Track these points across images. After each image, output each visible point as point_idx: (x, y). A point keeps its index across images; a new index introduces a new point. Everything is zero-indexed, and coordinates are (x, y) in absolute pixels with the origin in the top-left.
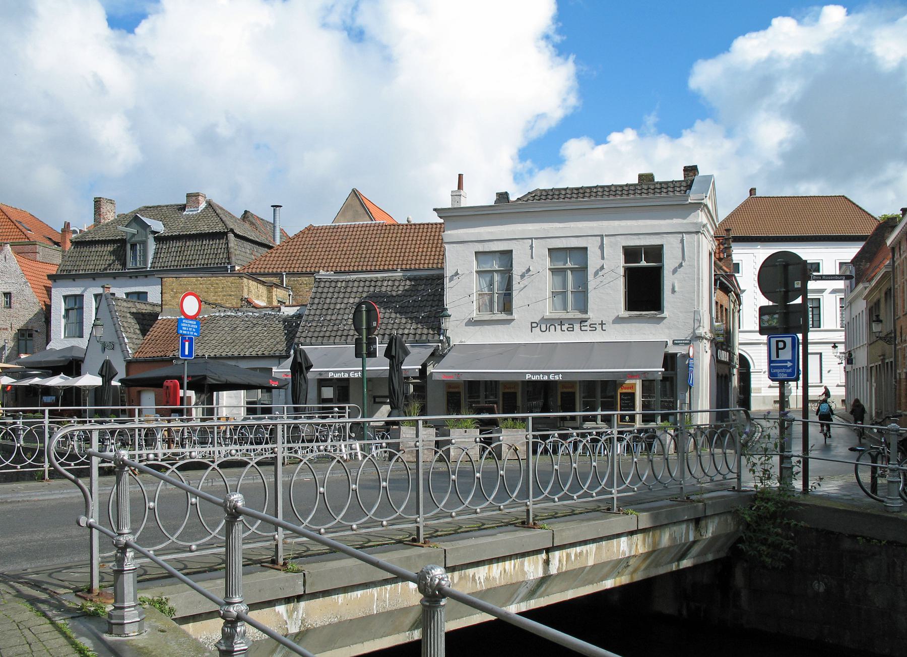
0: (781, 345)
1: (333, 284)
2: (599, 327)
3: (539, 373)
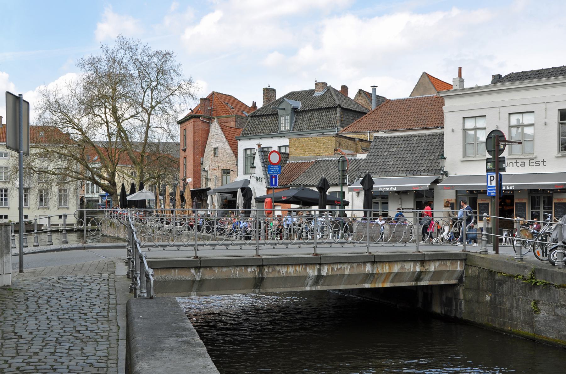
2: (542, 164)
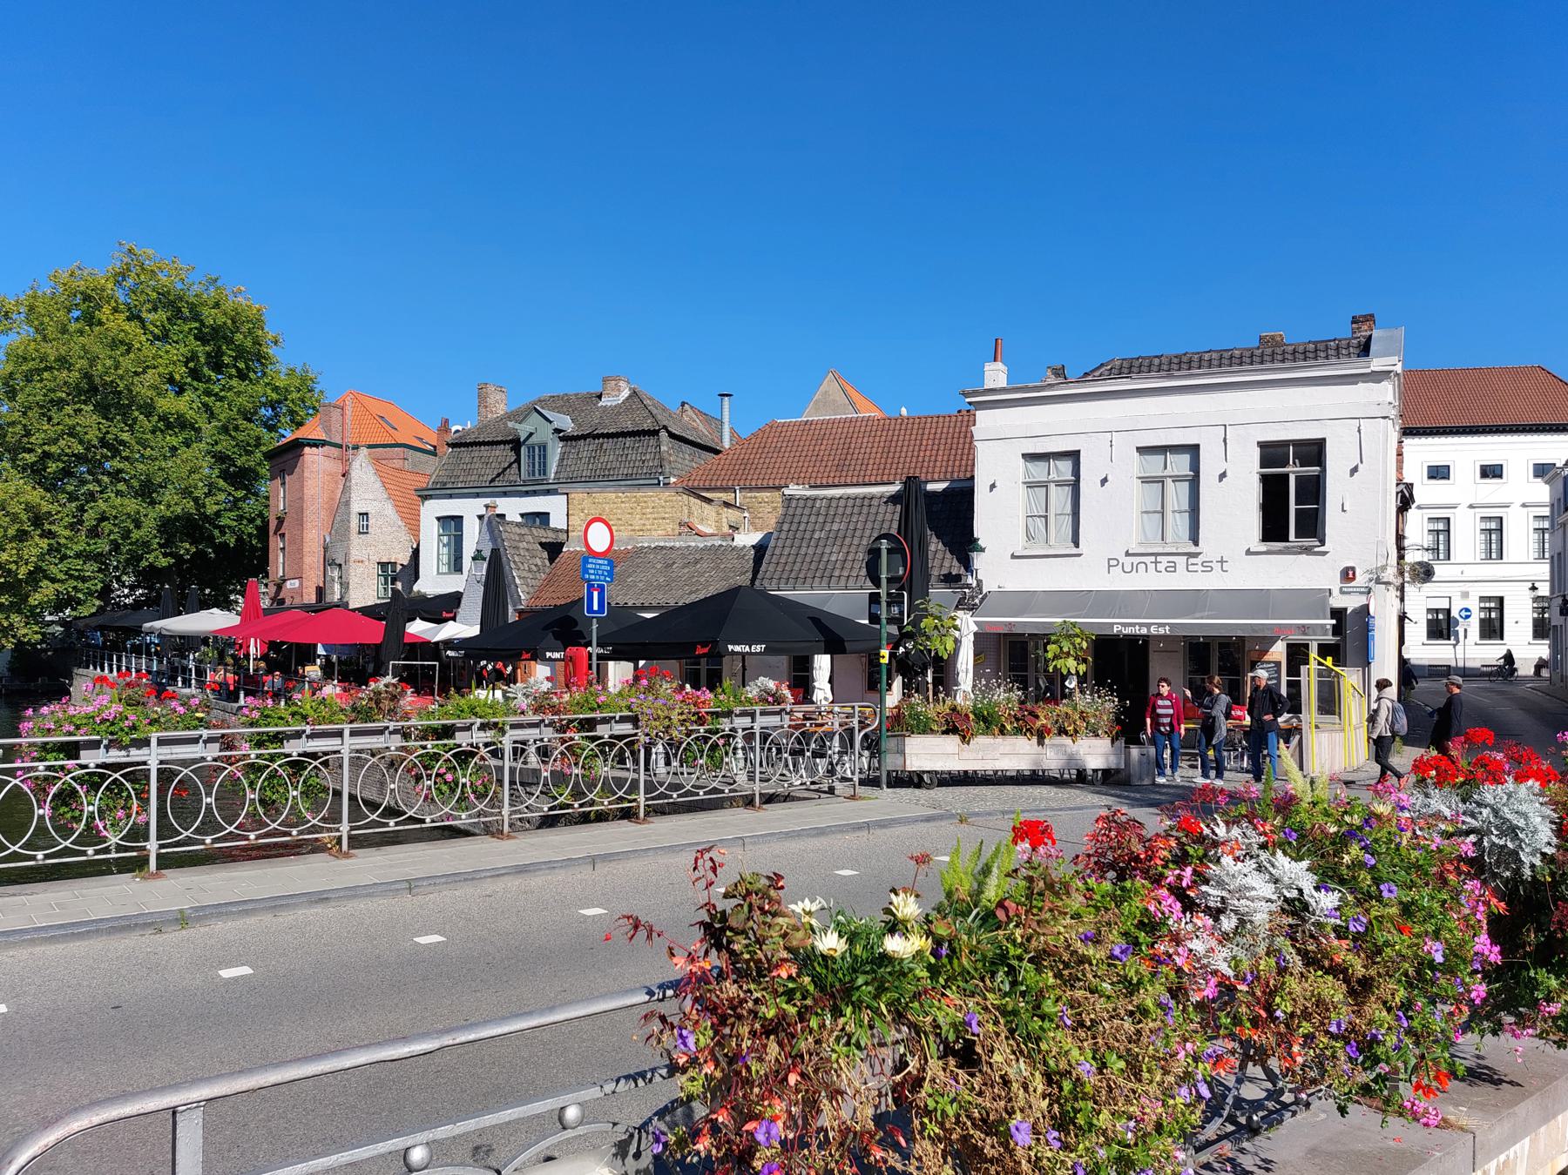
3: (1133, 625)
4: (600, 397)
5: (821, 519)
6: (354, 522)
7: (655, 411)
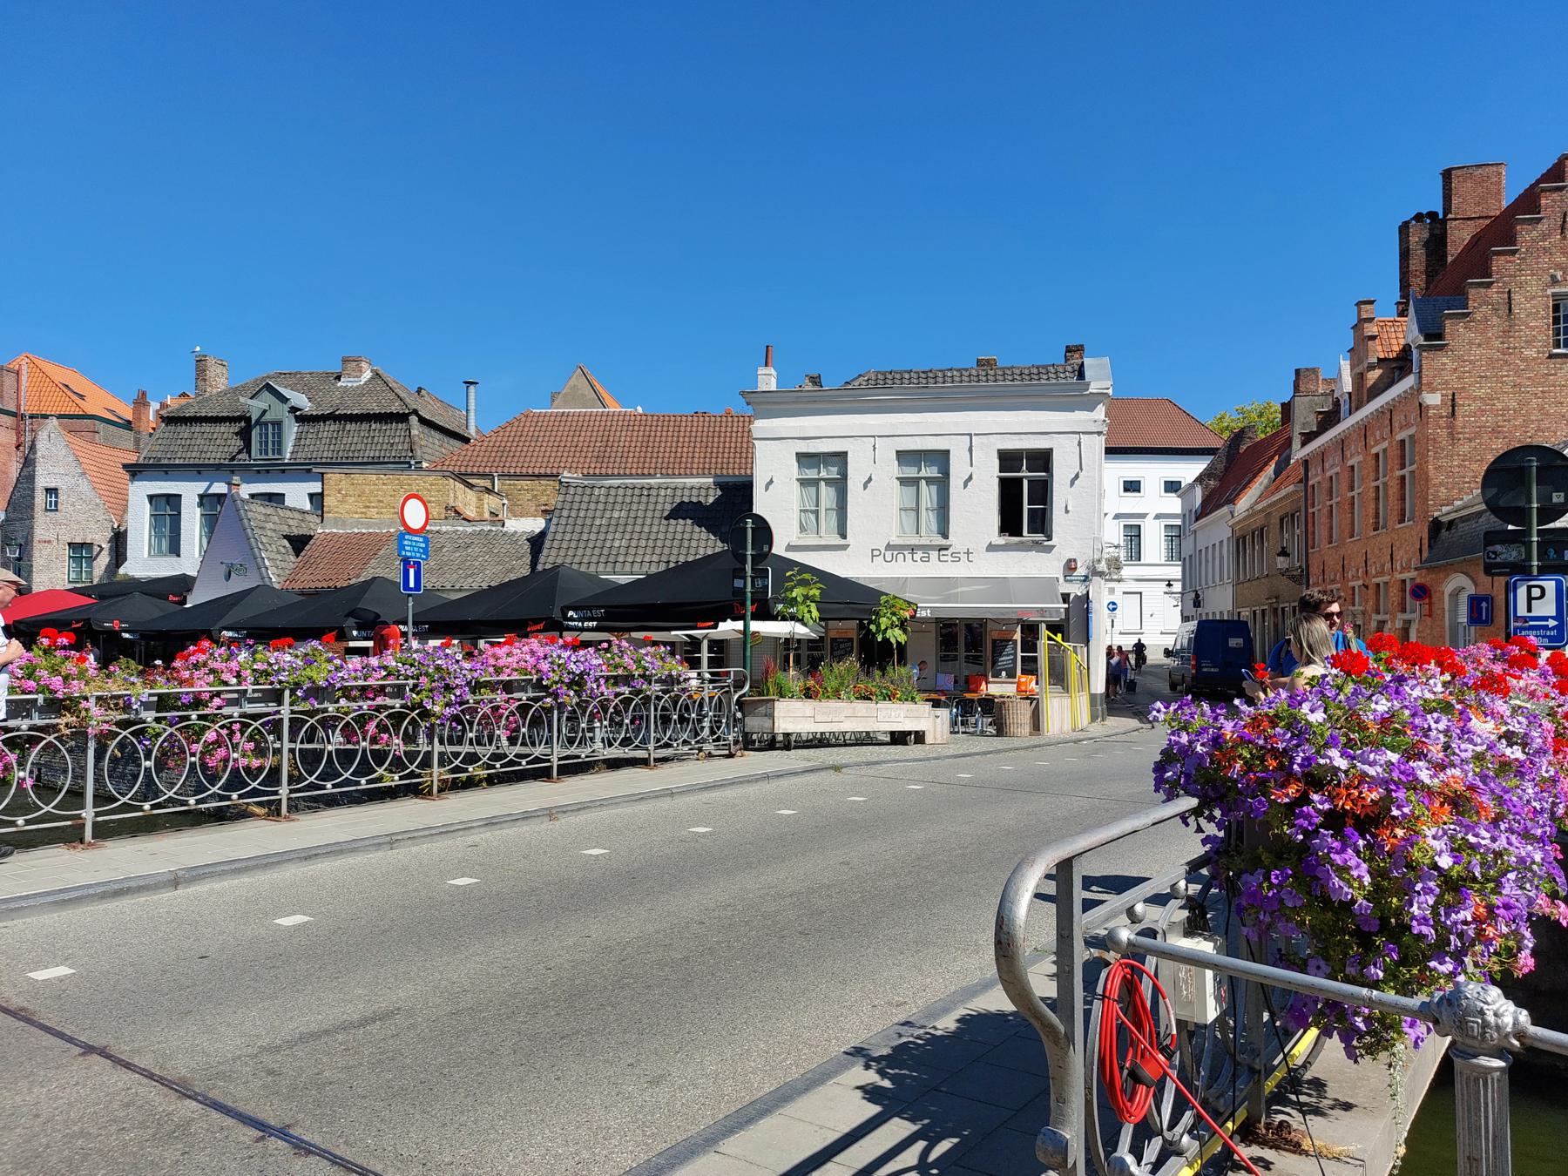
0: (1536, 592)
1: (588, 491)
4: (338, 378)
5: (601, 506)
6: (40, 499)
7: (402, 395)
